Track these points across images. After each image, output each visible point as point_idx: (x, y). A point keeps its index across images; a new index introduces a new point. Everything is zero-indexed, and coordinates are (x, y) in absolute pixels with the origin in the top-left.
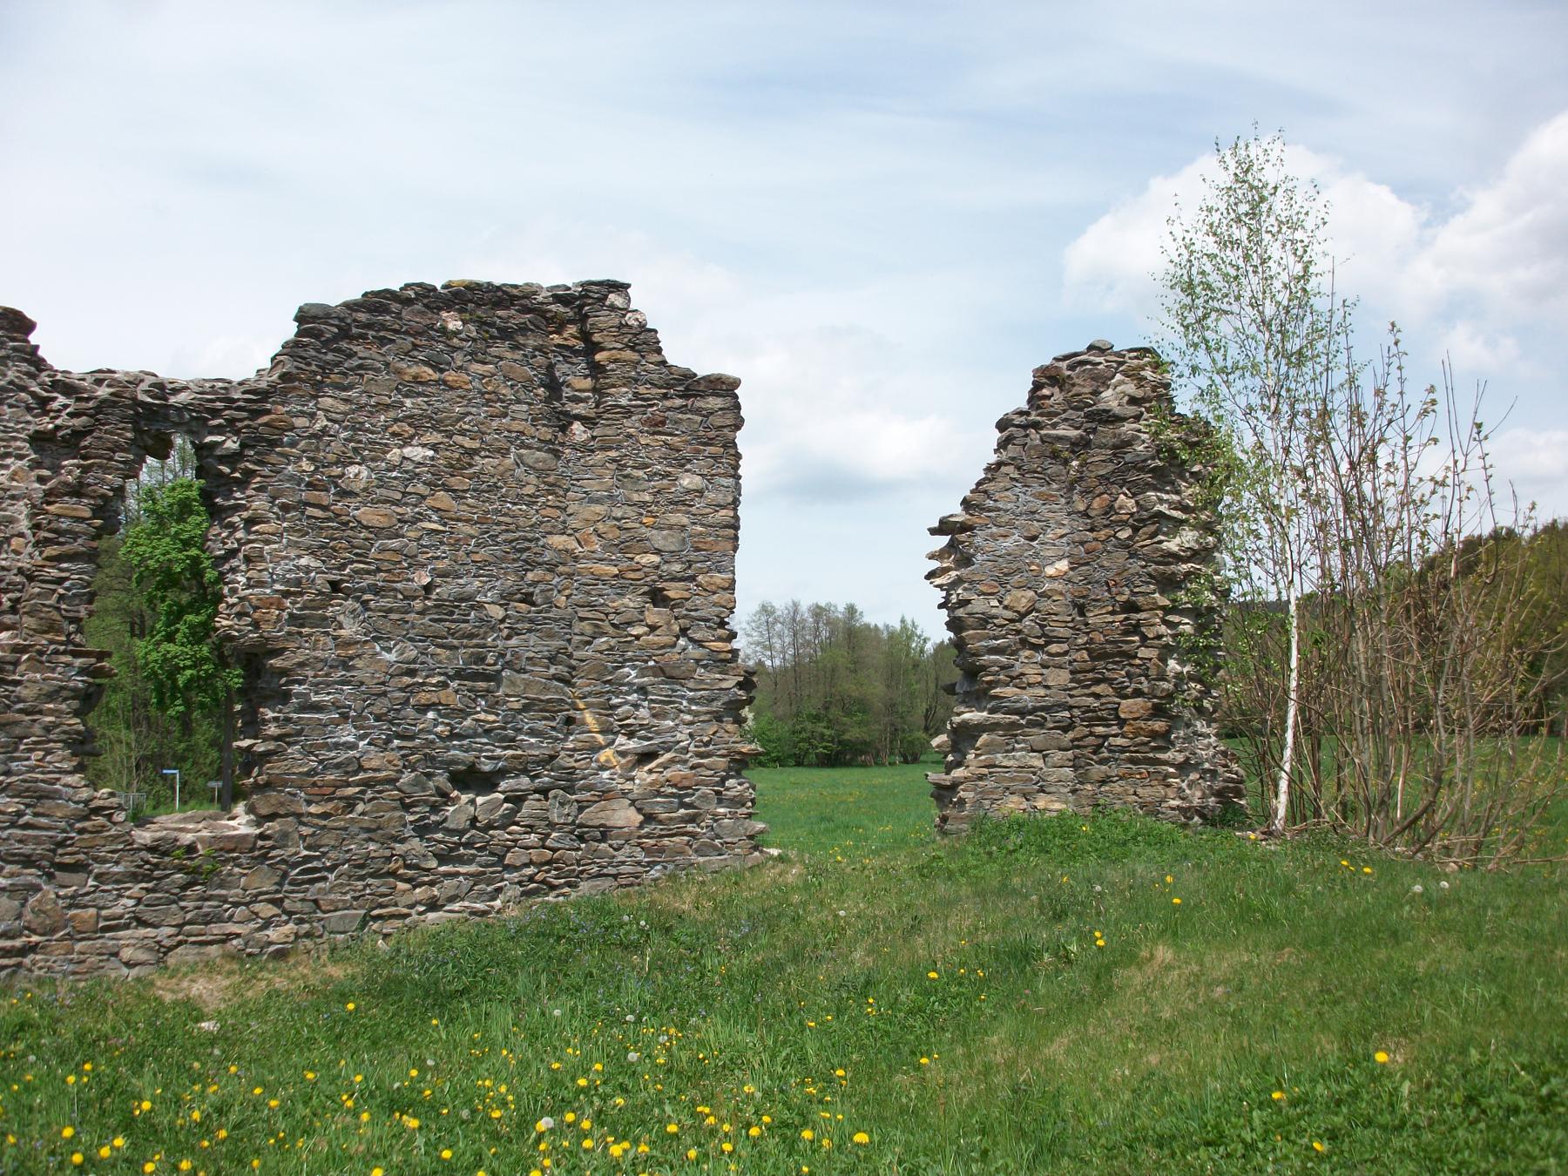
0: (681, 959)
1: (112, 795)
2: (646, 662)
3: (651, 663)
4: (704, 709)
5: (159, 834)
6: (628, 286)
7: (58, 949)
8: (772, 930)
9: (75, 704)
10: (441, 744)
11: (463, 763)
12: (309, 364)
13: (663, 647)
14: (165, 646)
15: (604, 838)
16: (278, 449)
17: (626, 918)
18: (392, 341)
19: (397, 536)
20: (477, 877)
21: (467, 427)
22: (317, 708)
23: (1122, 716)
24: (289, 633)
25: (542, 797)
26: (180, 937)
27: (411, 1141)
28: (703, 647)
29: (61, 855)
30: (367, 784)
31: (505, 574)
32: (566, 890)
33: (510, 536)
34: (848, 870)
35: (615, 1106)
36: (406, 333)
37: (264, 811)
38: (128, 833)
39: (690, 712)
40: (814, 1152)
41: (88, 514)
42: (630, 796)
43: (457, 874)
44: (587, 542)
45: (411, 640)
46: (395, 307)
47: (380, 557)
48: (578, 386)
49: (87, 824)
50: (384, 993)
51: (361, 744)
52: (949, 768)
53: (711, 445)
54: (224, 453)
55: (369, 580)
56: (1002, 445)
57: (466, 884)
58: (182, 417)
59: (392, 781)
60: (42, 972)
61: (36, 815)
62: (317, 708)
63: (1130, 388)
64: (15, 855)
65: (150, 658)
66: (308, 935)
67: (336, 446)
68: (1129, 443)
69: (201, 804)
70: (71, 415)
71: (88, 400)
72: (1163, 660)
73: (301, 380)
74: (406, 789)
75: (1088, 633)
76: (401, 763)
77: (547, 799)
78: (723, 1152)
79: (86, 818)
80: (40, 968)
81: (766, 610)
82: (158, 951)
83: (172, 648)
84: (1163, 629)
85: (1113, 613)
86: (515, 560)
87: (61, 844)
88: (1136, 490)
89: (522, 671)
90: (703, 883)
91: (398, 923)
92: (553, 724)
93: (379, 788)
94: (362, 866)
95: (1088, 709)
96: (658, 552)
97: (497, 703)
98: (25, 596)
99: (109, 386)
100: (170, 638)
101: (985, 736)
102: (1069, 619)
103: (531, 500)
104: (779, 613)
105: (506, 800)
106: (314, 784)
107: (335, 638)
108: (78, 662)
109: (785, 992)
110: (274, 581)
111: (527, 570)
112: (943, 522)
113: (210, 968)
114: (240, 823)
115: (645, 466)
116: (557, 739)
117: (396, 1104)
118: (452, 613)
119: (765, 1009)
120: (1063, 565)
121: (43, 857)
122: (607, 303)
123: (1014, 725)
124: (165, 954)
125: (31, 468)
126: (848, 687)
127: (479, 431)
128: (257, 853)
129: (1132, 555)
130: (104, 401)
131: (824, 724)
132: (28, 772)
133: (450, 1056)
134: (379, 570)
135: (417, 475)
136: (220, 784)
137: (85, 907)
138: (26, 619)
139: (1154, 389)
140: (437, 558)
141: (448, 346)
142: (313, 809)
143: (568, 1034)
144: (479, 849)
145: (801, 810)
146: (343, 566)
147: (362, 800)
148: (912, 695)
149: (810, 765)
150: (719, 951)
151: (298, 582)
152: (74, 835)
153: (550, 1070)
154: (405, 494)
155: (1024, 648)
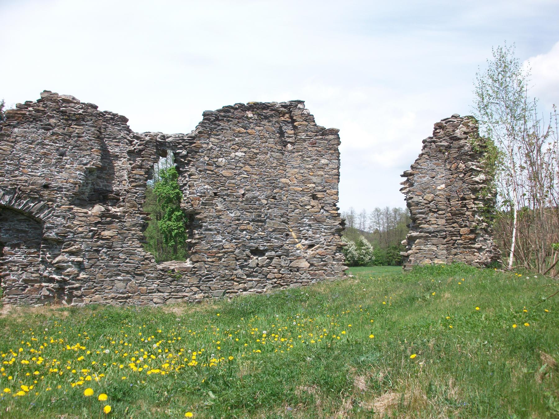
3: (312, 217)
6: (304, 102)
9: (140, 228)
11: (254, 247)
12: (207, 128)
13: (316, 212)
14: (168, 222)
15: (298, 271)
18: (232, 121)
19: (234, 179)
20: (258, 282)
22: (210, 230)
23: (461, 233)
24: (202, 208)
30: (225, 253)
32: (286, 286)
33: (269, 179)
36: (236, 118)
37: (195, 260)
38: (155, 265)
39: (324, 232)
41: (144, 174)
43: (252, 280)
45: (239, 210)
46: (232, 111)
47: (229, 185)
49: (144, 262)
50: (229, 313)
51: (223, 241)
55: (226, 192)
56: (424, 147)
57: (255, 283)
58: (170, 145)
59: (233, 252)
60: (132, 304)
61: (130, 259)
62: (210, 230)
63: (465, 129)
65: (163, 226)
66: (207, 297)
67: (215, 153)
68: (463, 147)
70: (139, 145)
72: (474, 215)
73: (205, 133)
75: (451, 207)
76: (235, 247)
77: (280, 259)
79: (144, 261)
83: (170, 223)
84: (473, 206)
85: (458, 201)
86: (270, 186)
87: (137, 268)
88: (465, 161)
91: (234, 294)
92: (282, 236)
93: (229, 254)
94: (223, 277)
95: (451, 232)
96: (314, 183)
98: (126, 197)
99: (149, 137)
100: (170, 220)
101: (418, 240)
102: (445, 203)
103: (275, 168)
104: (382, 211)
105: (268, 259)
106: (209, 252)
107: (215, 209)
108: (141, 216)
110: (197, 193)
112: (405, 173)
113: (179, 305)
114: (188, 264)
115: (310, 157)
116: (283, 240)
118: (251, 202)
120: (443, 186)
121: (132, 271)
123: (427, 237)
124: (166, 301)
125: (128, 161)
129: (464, 182)
130: (148, 141)
134: (228, 189)
137: (144, 286)
138: (127, 204)
139: (472, 129)
140: (246, 186)
142: (209, 260)
146: (218, 188)
149: (393, 265)
151: (204, 193)
154: (236, 166)
155: (430, 212)
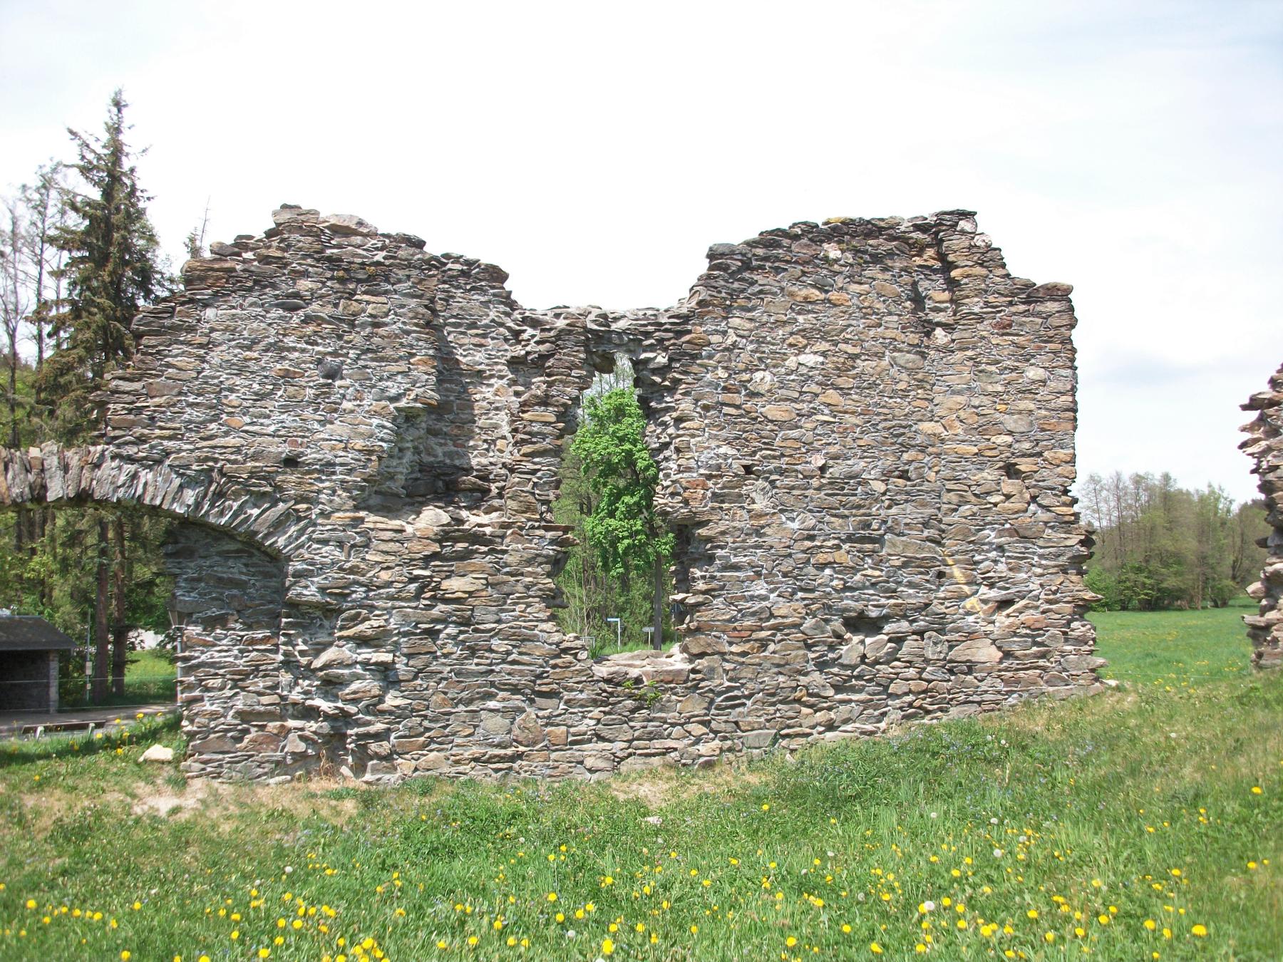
0: (1035, 772)
1: (577, 638)
2: (1003, 525)
3: (1007, 526)
4: (1052, 563)
5: (613, 669)
6: (975, 213)
7: (538, 757)
8: (1112, 748)
9: (548, 567)
10: (836, 595)
11: (854, 610)
13: (1017, 512)
15: (970, 671)
16: (698, 362)
17: (989, 738)
19: (797, 427)
20: (866, 704)
21: (849, 336)
22: (736, 567)
25: (918, 638)
26: (630, 750)
27: (817, 916)
28: (1050, 511)
29: (540, 685)
30: (777, 628)
31: (885, 455)
32: (939, 714)
33: (888, 424)
34: (1176, 698)
35: (983, 894)
36: (796, 262)
37: (695, 651)
39: (1040, 566)
40: (1155, 939)
42: (991, 636)
43: (850, 701)
44: (951, 427)
45: (810, 511)
46: (786, 242)
48: (938, 299)
49: (558, 661)
51: (772, 596)
52: (1263, 611)
53: (1051, 342)
54: (656, 366)
57: (858, 709)
59: (797, 626)
60: (527, 775)
61: (520, 653)
62: (736, 567)
64: (505, 684)
65: (596, 530)
66: (730, 750)
67: (745, 357)
69: (638, 645)
70: (538, 343)
71: (549, 330)
74: (809, 632)
76: (804, 611)
78: (1076, 936)
79: (558, 656)
80: (526, 771)
81: (1093, 480)
82: (614, 761)
86: (892, 444)
87: (539, 676)
89: (901, 534)
90: (1053, 709)
91: (803, 740)
92: (927, 578)
93: (786, 631)
94: (773, 695)
96: (1011, 433)
97: (881, 561)
98: (508, 484)
100: (611, 514)
103: (904, 394)
105: (890, 640)
106: (735, 629)
107: (749, 511)
108: (549, 535)
109: (1125, 802)
110: (699, 467)
111: (903, 452)
113: (653, 774)
116: (931, 590)
117: (803, 886)
118: (843, 489)
119: (1108, 816)
121: (526, 686)
122: (958, 229)
124: (619, 763)
125: (510, 386)
126: (1166, 543)
127: (859, 339)
128: (689, 684)
130: (561, 331)
131: (1145, 574)
132: (514, 620)
133: (846, 849)
134: (783, 455)
135: (811, 377)
136: (653, 629)
137: (558, 725)
138: (509, 502)
140: (829, 444)
141: (831, 271)
142: (734, 649)
143: (942, 832)
144: (868, 681)
145: (1127, 647)
146: (754, 453)
147: (774, 641)
148: (1221, 549)
149: (1134, 610)
150: (1067, 766)
151: (719, 467)
152: (548, 669)
153: (928, 862)
154: (801, 393)
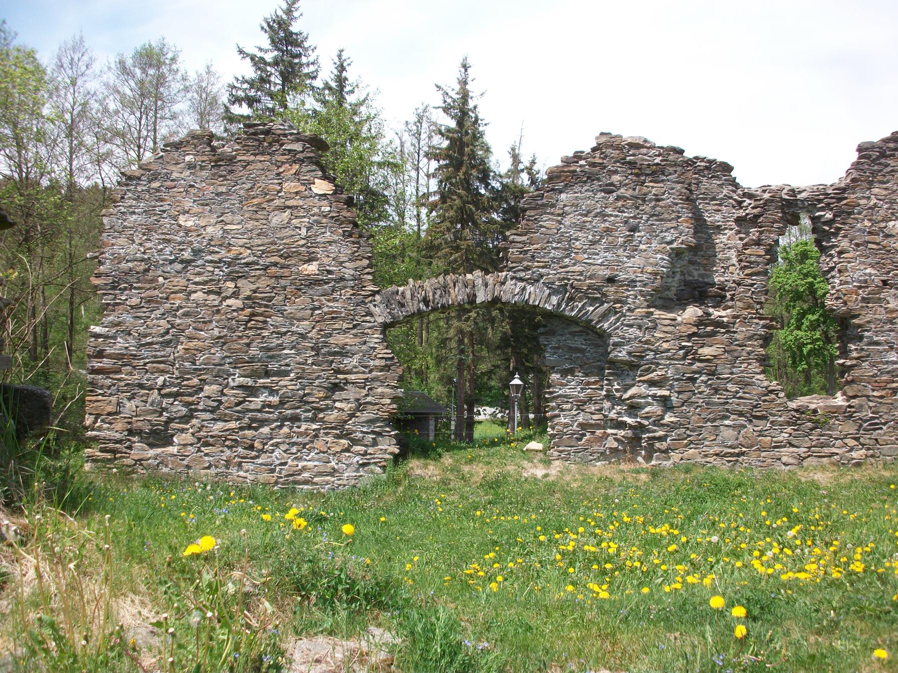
9: (761, 342)
14: (796, 332)
22: (877, 343)
37: (850, 394)
49: (767, 398)
61: (744, 393)
62: (877, 343)
66: (872, 456)
79: (766, 395)
87: (755, 407)
98: (737, 292)
100: (798, 328)
106: (876, 381)
107: (886, 309)
108: (762, 322)
113: (823, 468)
114: (840, 400)
121: (747, 412)
125: (736, 234)
130: (767, 200)
138: (738, 303)
142: (875, 394)
146: (888, 273)
151: (866, 281)
